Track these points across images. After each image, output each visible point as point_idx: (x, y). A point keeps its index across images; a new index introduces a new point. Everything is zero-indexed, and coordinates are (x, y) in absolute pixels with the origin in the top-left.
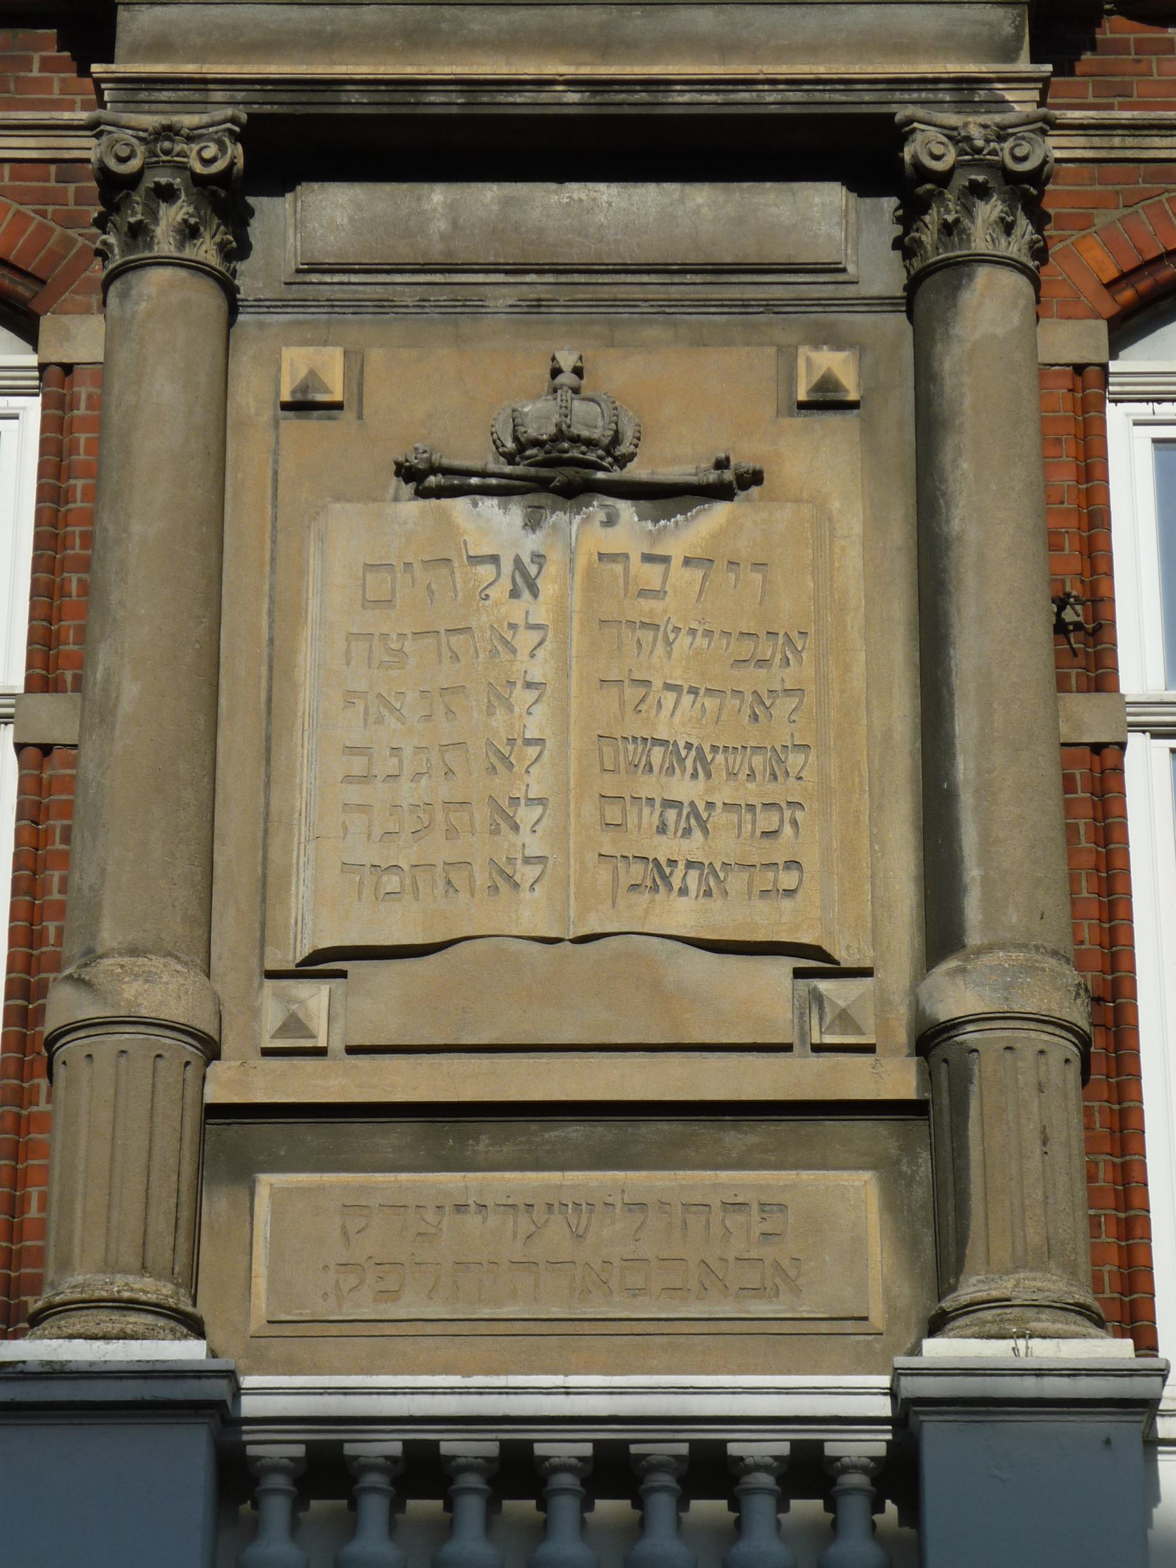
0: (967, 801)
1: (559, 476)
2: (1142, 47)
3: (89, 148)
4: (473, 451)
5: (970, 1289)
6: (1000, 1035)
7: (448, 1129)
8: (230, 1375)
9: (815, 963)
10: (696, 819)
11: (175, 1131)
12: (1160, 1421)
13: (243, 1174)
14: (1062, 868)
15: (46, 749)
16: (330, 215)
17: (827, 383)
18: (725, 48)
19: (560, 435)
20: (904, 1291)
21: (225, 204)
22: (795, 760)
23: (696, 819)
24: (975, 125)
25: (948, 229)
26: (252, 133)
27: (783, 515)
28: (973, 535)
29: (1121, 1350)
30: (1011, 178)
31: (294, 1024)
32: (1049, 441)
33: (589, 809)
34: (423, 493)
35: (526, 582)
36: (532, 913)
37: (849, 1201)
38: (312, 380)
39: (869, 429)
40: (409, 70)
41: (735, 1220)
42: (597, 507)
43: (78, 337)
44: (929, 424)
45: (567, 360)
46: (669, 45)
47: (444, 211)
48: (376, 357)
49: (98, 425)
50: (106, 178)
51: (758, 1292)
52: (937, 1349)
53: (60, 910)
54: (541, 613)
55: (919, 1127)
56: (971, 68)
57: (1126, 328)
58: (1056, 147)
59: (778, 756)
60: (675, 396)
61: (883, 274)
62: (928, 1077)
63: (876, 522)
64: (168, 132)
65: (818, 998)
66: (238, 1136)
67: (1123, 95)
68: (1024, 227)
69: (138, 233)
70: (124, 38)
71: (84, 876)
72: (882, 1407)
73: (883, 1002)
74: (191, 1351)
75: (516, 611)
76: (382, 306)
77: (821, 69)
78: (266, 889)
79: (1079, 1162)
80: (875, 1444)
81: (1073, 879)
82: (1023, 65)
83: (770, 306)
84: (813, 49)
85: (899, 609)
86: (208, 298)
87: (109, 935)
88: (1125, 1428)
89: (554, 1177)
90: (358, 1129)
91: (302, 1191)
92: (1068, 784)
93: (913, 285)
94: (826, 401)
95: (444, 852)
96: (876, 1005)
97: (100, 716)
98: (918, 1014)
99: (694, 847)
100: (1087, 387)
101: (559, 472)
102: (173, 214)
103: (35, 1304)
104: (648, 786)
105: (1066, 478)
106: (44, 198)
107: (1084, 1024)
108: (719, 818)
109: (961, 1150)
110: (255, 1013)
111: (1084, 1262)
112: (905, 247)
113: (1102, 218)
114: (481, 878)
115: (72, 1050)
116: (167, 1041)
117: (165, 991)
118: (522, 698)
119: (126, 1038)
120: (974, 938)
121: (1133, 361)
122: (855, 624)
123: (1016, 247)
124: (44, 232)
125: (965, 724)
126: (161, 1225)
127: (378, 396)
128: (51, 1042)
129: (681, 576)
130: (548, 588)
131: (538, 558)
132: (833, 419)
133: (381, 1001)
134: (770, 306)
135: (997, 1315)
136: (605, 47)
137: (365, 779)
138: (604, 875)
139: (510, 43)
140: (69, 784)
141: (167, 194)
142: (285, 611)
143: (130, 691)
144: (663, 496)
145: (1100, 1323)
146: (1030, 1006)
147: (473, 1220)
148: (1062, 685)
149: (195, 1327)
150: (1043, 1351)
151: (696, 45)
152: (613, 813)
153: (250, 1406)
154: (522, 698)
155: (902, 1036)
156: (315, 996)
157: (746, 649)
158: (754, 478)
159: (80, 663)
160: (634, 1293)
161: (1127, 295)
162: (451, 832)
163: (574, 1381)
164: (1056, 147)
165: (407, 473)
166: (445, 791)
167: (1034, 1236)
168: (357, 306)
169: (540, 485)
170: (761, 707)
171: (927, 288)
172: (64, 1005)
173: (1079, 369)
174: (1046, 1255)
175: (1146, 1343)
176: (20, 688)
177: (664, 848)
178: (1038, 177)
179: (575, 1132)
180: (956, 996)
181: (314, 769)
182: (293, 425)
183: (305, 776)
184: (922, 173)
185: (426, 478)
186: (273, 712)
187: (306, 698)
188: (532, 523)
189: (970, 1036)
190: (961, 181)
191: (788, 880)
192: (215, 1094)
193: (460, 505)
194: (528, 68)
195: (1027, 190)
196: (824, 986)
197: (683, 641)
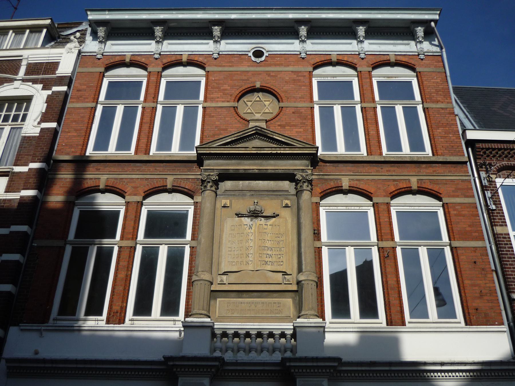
0: (303, 254)
1: (255, 215)
2: (324, 166)
3: (200, 177)
4: (245, 212)
5: (303, 313)
6: (307, 282)
7: (240, 294)
8: (213, 323)
9: (285, 273)
10: (271, 256)
11: (207, 293)
12: (327, 335)
13: (215, 299)
14: (314, 262)
15: (193, 247)
16: (228, 184)
17: (287, 204)
18: (275, 166)
19: (255, 210)
20: (295, 313)
21: (216, 183)
22: (283, 249)
23: (271, 256)
24: (304, 174)
25: (301, 186)
26: (219, 175)
27: (282, 219)
28: (304, 222)
29: (321, 320)
30: (308, 181)
31: (222, 281)
32: (313, 211)
33: (258, 254)
34: (238, 217)
35: (251, 228)
36: (251, 267)
37: (289, 302)
38: (226, 204)
39: (292, 209)
40: (238, 168)
41: (274, 305)
42: (259, 219)
43: (198, 199)
44: (299, 209)
45: (256, 201)
46: (267, 165)
47: (242, 184)
48: (233, 201)
49: (200, 209)
50: (202, 180)
51: (277, 313)
52: (299, 320)
53: (194, 267)
54: (252, 231)
55: (297, 293)
56: (303, 168)
57: (322, 198)
58: (314, 177)
59: (280, 249)
60: (269, 206)
61: (294, 192)
62: (298, 287)
63: (292, 221)
64: (209, 175)
65: (285, 278)
66: (215, 294)
67: (321, 171)
68: (310, 186)
69: (205, 187)
70: (204, 164)
71: (197, 263)
72: (292, 327)
73: (293, 278)
74: (208, 320)
75: (249, 231)
76: (234, 195)
77: (286, 168)
78: (219, 264)
79: (316, 297)
80: (291, 332)
81: (316, 264)
82: (310, 168)
83: (280, 195)
84: (285, 166)
85: (295, 231)
86: (213, 194)
87: (200, 270)
88: (322, 329)
89: (253, 299)
90: (229, 293)
91: (222, 301)
92: (315, 252)
93: (297, 193)
94: (287, 206)
95: (240, 260)
96: (292, 279)
97: (199, 243)
98: (297, 279)
99: (270, 259)
100: (318, 205)
101: (255, 214)
102: (210, 184)
103: (190, 314)
104: (265, 252)
105: (315, 215)
106: (195, 183)
107: (317, 281)
108: (273, 256)
109: (302, 296)
110: (217, 279)
111: (317, 310)
112: (296, 188)
113: (319, 185)
114: (245, 263)
115: (195, 283)
116: (206, 282)
117: (206, 276)
118: (250, 241)
119: (201, 282)
120: (304, 270)
121: (322, 202)
122: (290, 232)
123: (309, 188)
124: (195, 187)
125: (303, 245)
126: (205, 305)
127: (234, 205)
128: (193, 282)
129: (269, 227)
130: (253, 228)
131: (252, 225)
132: (288, 208)
133: (232, 278)
134: (280, 195)
135: (306, 316)
136: (261, 166)
137: (231, 251)
138: (259, 263)
139: (249, 165)
140: (195, 252)
141: (209, 182)
142: (222, 231)
143: (203, 240)
144: (267, 217)
145: (318, 317)
146: (310, 279)
147: (243, 304)
148: (314, 240)
149: (209, 317)
150: (311, 320)
151: (271, 165)
152: (261, 255)
153: (215, 327)
154: (250, 241)
155: (295, 282)
156: (224, 277)
157: (277, 236)
158: (278, 215)
159: (197, 237)
160: (262, 313)
161: (322, 194)
162: (241, 258)
163: (255, 324)
164: (314, 177)
165: (236, 214)
166: (240, 253)
167: (310, 307)
168: (231, 195)
169: (253, 216)
170: (278, 242)
171: (298, 193)
172: (194, 278)
173: (316, 203)
174: (312, 309)
175: (324, 319)
176: (190, 240)
177: (267, 260)
178: (311, 180)
179: (255, 294)
180: (301, 277)
181: (225, 250)
182: (223, 209)
183: (224, 251)
184: (298, 180)
185: (239, 215)
186: (220, 243)
187: (224, 241)
188: (251, 221)
189: (303, 282)
190: (302, 181)
191: (282, 263)
192: (212, 289)
193: (243, 218)
194: (252, 168)
195: (310, 182)
196: (286, 276)
197: (269, 235)
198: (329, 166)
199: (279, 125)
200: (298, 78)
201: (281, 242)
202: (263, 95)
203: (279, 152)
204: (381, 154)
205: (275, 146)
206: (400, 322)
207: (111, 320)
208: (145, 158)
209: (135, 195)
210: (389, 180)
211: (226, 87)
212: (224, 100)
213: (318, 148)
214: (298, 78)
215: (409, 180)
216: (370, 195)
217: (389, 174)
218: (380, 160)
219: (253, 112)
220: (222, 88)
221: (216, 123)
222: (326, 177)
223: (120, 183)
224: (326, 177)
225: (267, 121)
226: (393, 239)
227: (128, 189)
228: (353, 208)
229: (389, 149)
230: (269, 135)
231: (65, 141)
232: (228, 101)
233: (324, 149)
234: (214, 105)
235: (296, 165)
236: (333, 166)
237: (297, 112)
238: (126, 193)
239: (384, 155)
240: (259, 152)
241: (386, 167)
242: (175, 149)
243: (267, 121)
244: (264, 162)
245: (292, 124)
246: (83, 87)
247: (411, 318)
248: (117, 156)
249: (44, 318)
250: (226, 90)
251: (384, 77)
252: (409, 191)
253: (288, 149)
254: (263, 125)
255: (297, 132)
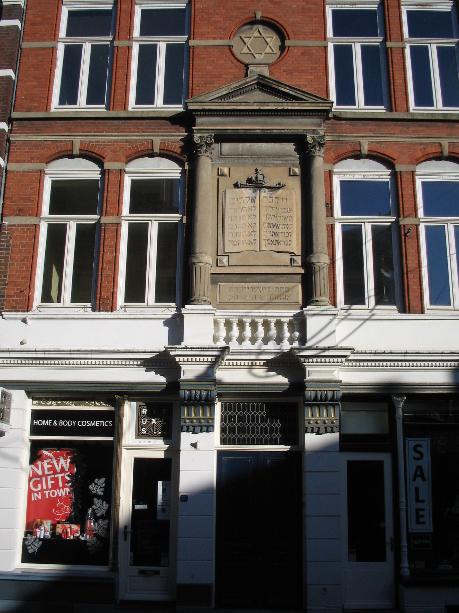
2: (339, 124)
16: (227, 147)
18: (281, 125)
24: (315, 136)
46: (272, 124)
60: (273, 174)
70: (197, 123)
76: (233, 161)
77: (294, 128)
84: (293, 125)
101: (255, 184)
113: (333, 149)
114: (247, 243)
137: (232, 228)
147: (247, 289)
151: (276, 124)
168: (229, 160)
185: (236, 186)
188: (254, 192)
191: (289, 243)
194: (253, 128)
198: (346, 124)
199: (284, 71)
200: (307, 6)
201: (289, 219)
202: (264, 29)
203: (286, 108)
204: (408, 110)
205: (285, 101)
206: (419, 308)
207: (101, 307)
208: (123, 114)
209: (116, 161)
210: (416, 144)
211: (217, 18)
212: (216, 36)
213: (332, 103)
214: (307, 6)
215: (440, 144)
216: (392, 161)
217: (416, 136)
218: (405, 118)
219: (252, 52)
220: (213, 19)
221: (208, 67)
222: (342, 139)
223: (96, 146)
224: (342, 139)
225: (270, 65)
226: (416, 216)
227: (108, 154)
228: (372, 176)
229: (418, 103)
230: (274, 86)
231: (25, 93)
232: (221, 38)
233: (338, 104)
234: (203, 43)
235: (306, 125)
236: (350, 125)
237: (306, 51)
238: (104, 158)
239: (411, 111)
240: (262, 108)
241: (413, 127)
242: (159, 105)
243: (270, 65)
244: (269, 120)
245: (301, 68)
246: (37, 19)
247: (431, 304)
248: (89, 112)
249: (26, 306)
250: (217, 22)
251: (416, 5)
252: (439, 157)
253: (297, 104)
254: (266, 72)
255: (307, 80)
